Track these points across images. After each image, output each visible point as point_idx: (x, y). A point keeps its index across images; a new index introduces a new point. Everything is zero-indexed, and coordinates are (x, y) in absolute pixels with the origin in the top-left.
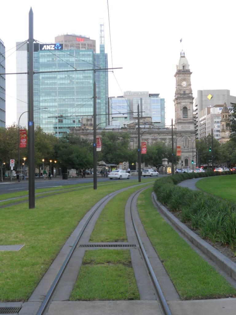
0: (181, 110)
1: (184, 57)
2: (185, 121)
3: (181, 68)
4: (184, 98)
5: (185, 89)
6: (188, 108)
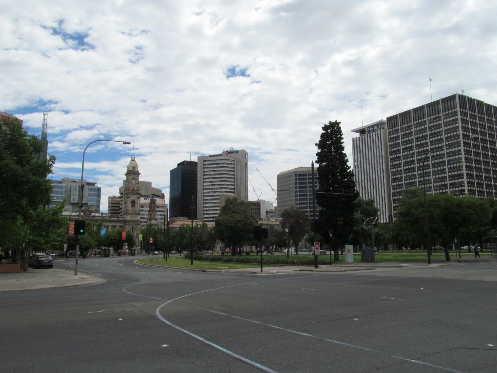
0: (137, 203)
1: (134, 160)
2: (133, 212)
3: (131, 169)
4: (133, 194)
5: (134, 186)
6: (136, 202)
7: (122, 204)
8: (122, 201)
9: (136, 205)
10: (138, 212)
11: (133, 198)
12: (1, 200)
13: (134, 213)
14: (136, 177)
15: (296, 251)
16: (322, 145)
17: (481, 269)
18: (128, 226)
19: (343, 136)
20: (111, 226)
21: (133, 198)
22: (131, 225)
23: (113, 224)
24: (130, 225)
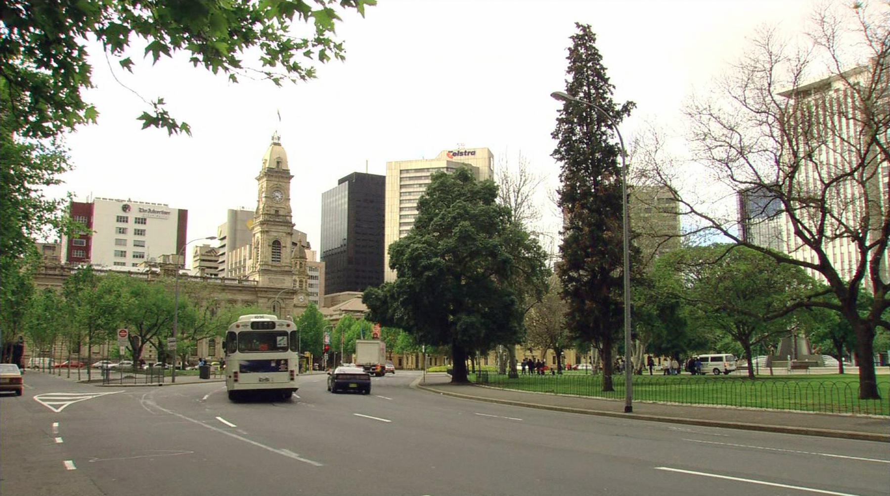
3: (274, 166)
6: (283, 245)
7: (224, 254)
8: (224, 246)
9: (283, 251)
10: (287, 269)
11: (275, 234)
12: (887, 297)
13: (279, 269)
14: (283, 184)
15: (769, 365)
16: (574, 56)
17: (101, 271)
18: (265, 300)
19: (571, 44)
20: (242, 301)
21: (275, 234)
22: (271, 301)
23: (230, 296)
24: (269, 299)
